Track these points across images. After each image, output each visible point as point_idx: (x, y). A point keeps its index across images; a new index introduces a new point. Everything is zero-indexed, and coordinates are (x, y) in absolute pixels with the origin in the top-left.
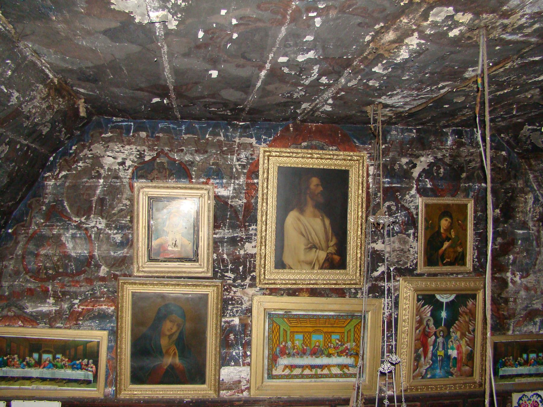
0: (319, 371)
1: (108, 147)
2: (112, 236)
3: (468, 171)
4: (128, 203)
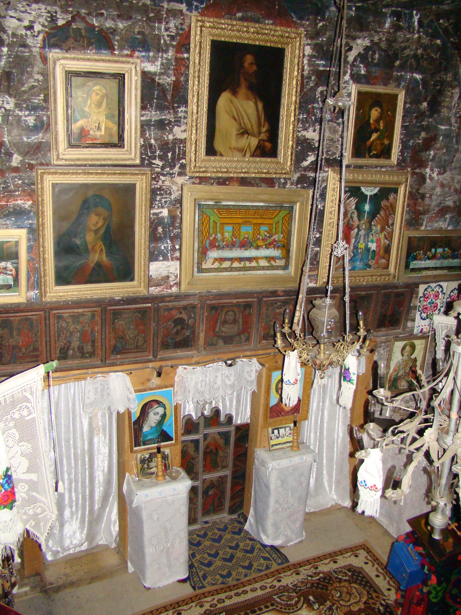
0: (248, 264)
2: (23, 118)
4: (41, 78)
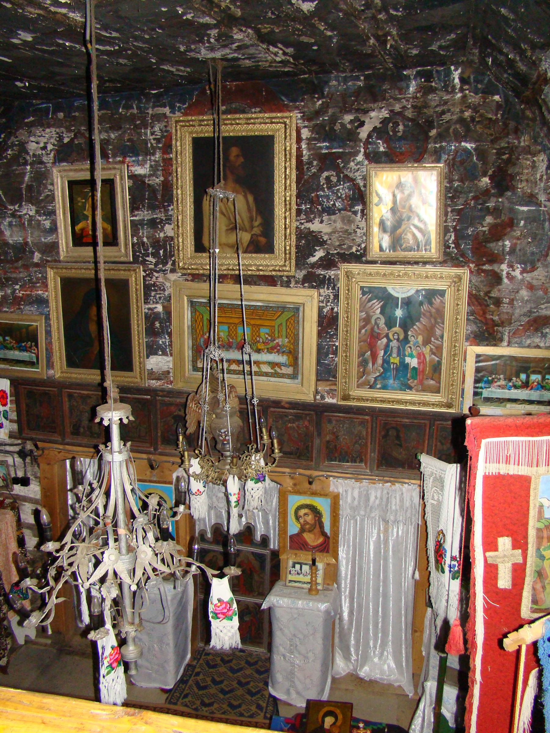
1: (31, 132)
2: (42, 222)
3: (439, 126)
